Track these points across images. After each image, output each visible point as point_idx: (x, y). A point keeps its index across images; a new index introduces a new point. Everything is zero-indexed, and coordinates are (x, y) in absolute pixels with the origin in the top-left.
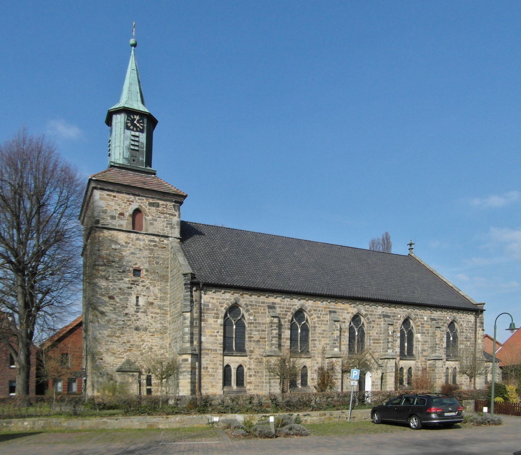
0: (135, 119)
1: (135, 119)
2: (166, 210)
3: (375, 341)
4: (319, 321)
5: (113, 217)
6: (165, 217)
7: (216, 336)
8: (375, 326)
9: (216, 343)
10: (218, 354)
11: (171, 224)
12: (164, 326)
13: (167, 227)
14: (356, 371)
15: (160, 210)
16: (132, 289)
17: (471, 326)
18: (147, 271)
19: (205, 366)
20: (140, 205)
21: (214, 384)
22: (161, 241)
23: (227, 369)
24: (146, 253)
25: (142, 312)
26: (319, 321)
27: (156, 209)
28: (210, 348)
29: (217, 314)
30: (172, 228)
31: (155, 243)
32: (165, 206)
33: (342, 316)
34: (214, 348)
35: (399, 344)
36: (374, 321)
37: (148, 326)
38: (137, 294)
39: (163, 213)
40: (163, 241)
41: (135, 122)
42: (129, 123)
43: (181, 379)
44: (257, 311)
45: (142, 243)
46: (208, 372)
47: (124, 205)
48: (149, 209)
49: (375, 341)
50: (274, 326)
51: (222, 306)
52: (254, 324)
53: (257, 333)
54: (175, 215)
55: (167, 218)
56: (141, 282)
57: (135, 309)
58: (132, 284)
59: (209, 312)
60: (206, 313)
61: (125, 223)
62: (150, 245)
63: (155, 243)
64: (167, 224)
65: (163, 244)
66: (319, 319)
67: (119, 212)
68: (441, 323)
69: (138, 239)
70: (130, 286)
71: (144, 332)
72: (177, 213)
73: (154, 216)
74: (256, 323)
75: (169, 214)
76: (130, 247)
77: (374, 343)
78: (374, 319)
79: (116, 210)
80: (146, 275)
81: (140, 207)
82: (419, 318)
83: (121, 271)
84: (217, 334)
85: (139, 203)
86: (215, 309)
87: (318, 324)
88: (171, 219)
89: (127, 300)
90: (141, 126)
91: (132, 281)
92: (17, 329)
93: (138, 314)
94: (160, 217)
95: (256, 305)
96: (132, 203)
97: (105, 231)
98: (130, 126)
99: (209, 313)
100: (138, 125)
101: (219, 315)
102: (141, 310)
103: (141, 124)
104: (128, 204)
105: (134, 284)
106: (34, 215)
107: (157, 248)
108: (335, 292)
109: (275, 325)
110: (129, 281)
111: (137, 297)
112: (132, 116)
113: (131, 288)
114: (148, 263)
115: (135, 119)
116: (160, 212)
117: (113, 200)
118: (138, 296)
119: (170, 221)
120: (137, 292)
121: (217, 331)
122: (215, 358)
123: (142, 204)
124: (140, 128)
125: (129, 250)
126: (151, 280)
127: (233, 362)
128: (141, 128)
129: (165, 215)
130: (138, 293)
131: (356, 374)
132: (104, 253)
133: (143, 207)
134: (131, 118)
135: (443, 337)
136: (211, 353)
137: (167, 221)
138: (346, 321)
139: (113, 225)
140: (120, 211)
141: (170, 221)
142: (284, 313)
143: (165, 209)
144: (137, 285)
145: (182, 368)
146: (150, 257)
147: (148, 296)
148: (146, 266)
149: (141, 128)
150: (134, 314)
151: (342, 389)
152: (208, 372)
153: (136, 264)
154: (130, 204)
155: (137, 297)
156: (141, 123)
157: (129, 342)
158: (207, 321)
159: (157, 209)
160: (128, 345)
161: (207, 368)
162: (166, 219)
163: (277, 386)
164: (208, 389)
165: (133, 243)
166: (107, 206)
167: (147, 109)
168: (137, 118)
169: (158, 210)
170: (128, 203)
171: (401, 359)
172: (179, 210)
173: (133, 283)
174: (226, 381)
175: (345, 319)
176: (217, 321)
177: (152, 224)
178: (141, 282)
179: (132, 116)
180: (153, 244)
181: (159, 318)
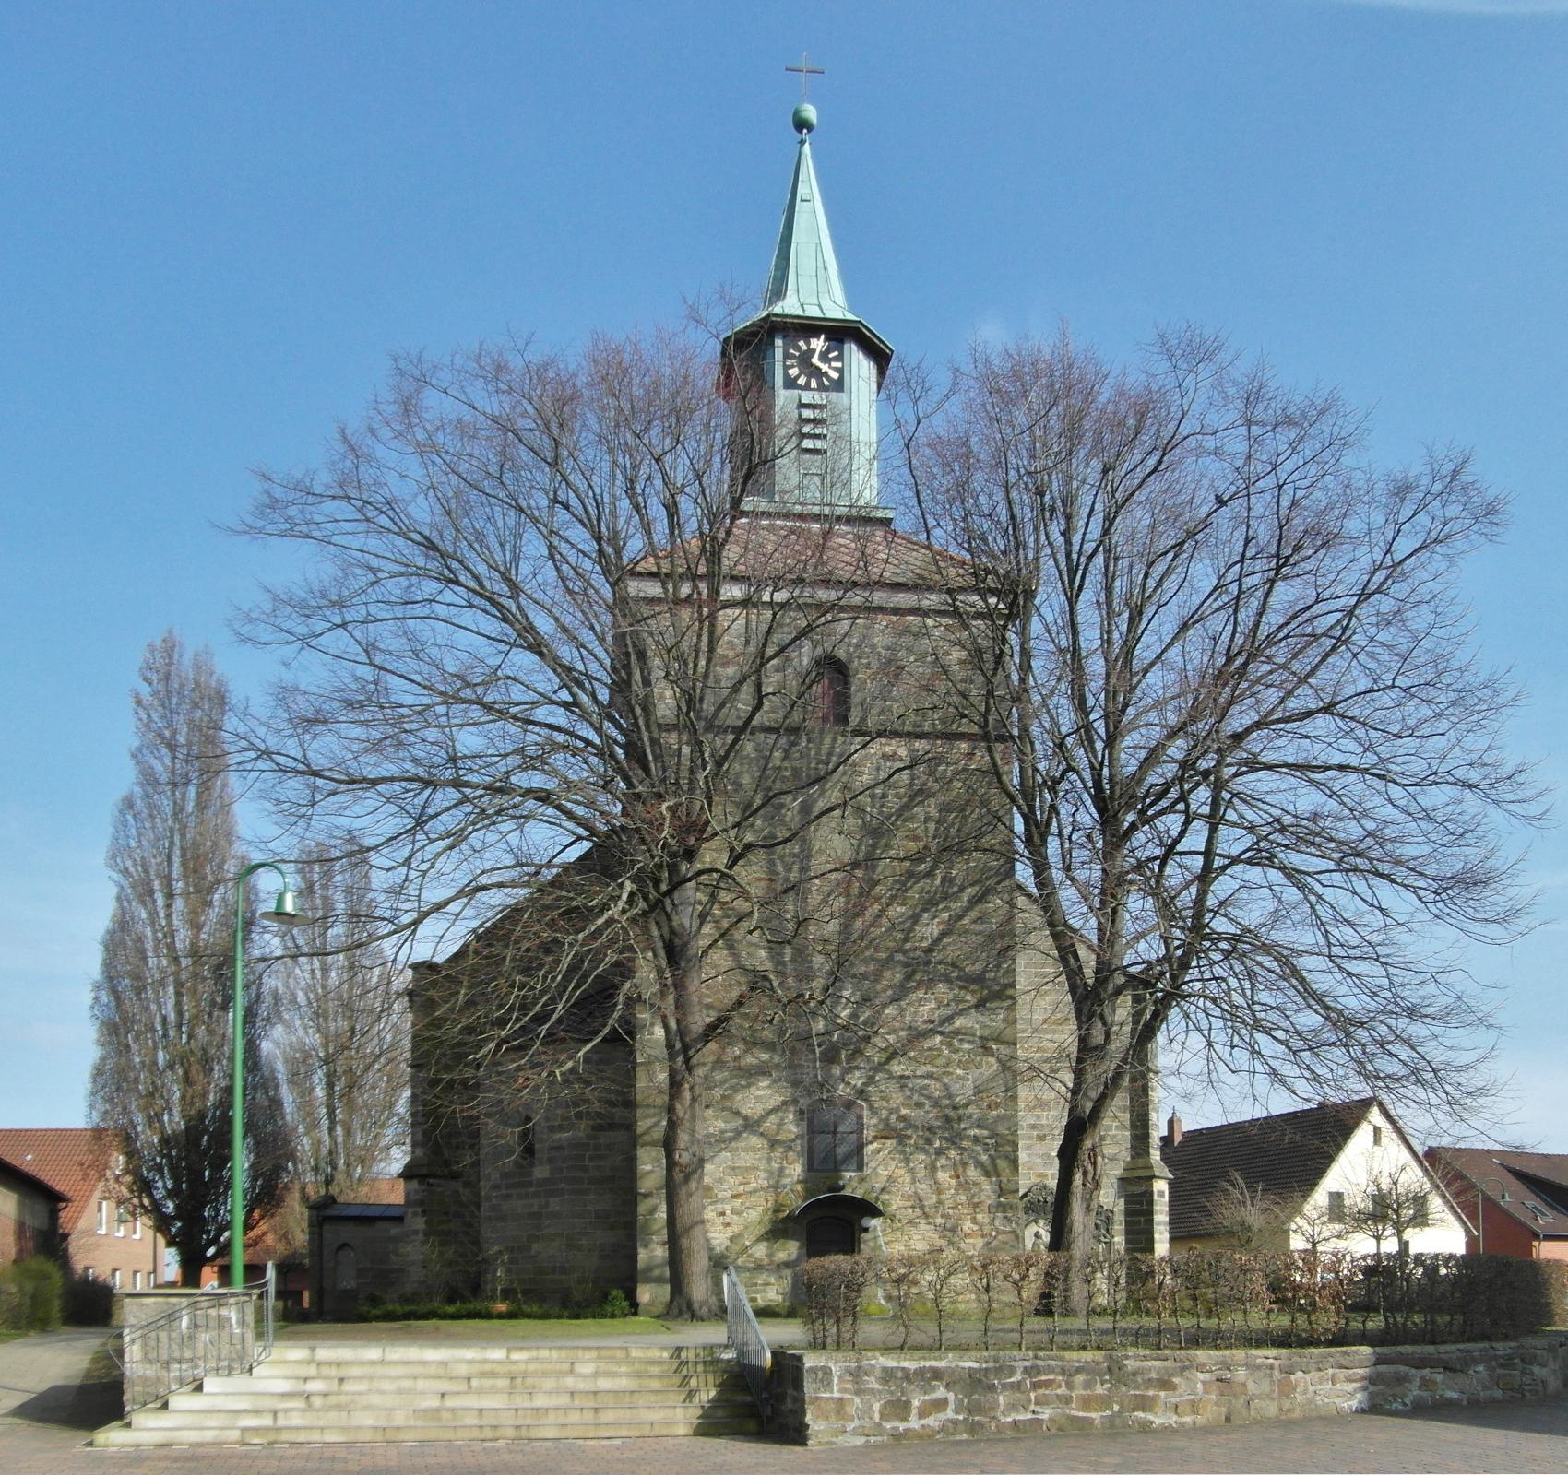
0: (812, 352)
1: (814, 351)
41: (815, 360)
42: (792, 366)
90: (836, 369)
92: (885, 1006)
98: (798, 377)
100: (824, 367)
103: (834, 364)
106: (519, 607)
108: (655, 1370)
112: (801, 343)
115: (812, 352)
124: (829, 378)
128: (835, 375)
132: (450, 1253)
134: (799, 349)
149: (835, 375)
151: (1012, 1331)
156: (836, 359)
167: (136, 1457)
168: (818, 344)
179: (801, 343)
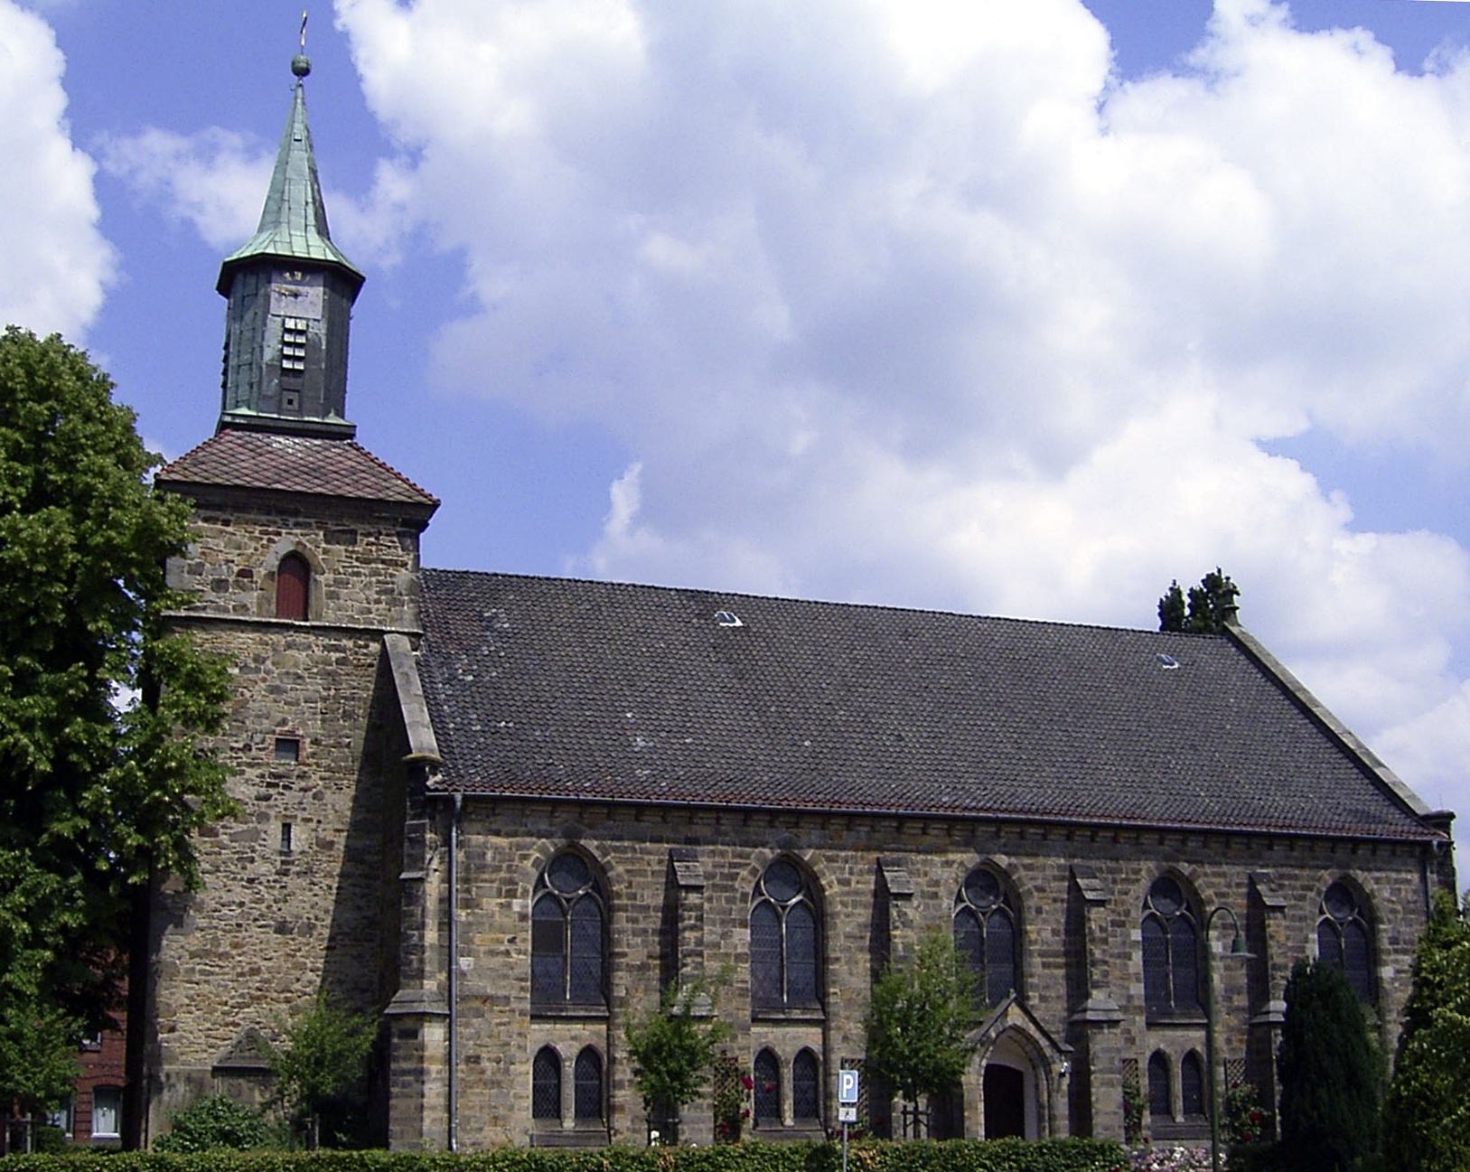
2: (377, 550)
3: (1051, 960)
4: (848, 894)
5: (220, 585)
6: (375, 573)
7: (507, 953)
8: (1046, 908)
9: (505, 977)
10: (513, 1011)
11: (392, 591)
12: (364, 918)
13: (378, 602)
14: (850, 1077)
15: (358, 552)
16: (272, 802)
17: (1410, 897)
18: (316, 742)
19: (471, 1052)
20: (299, 543)
21: (502, 1111)
22: (360, 647)
23: (548, 1059)
24: (316, 686)
25: (298, 874)
26: (848, 894)
27: (346, 551)
28: (489, 991)
29: (512, 882)
30: (395, 602)
31: (343, 655)
32: (372, 539)
33: (926, 874)
34: (501, 993)
35: (1140, 969)
36: (1041, 889)
37: (317, 918)
38: (286, 816)
39: (368, 562)
40: (366, 646)
43: (397, 1096)
44: (636, 867)
45: (302, 656)
46: (483, 1072)
47: (253, 544)
48: (325, 552)
49: (1051, 960)
50: (690, 918)
51: (525, 857)
52: (626, 911)
53: (639, 940)
54: (404, 565)
55: (380, 575)
56: (298, 777)
57: (278, 864)
58: (269, 785)
59: (486, 876)
60: (476, 880)
61: (253, 602)
62: (327, 662)
63: (343, 655)
64: (377, 593)
65: (365, 654)
66: (847, 889)
67: (236, 569)
68: (1294, 888)
69: (289, 646)
70: (263, 790)
71: (304, 940)
72: (409, 559)
73: (341, 570)
74: (632, 906)
75: (383, 562)
76: (268, 672)
77: (1045, 965)
78: (1039, 882)
79: (228, 561)
80: (313, 755)
81: (300, 549)
82: (1206, 875)
83: (240, 745)
84: (511, 947)
85: (296, 535)
86: (504, 865)
87: (844, 904)
88: (392, 575)
89: (255, 835)
91: (272, 775)
93: (285, 879)
94: (358, 574)
95: (634, 850)
96: (276, 538)
97: (199, 636)
99: (486, 881)
101: (517, 884)
102: (294, 869)
104: (265, 542)
105: (276, 785)
107: (349, 669)
109: (693, 914)
110: (263, 776)
111: (287, 828)
113: (267, 798)
114: (319, 717)
116: (357, 559)
117: (222, 532)
118: (288, 821)
119: (387, 583)
120: (286, 809)
121: (511, 936)
122: (504, 1024)
123: (304, 540)
125: (264, 680)
126: (328, 769)
127: (562, 1039)
129: (373, 565)
130: (288, 813)
131: (850, 1086)
133: (309, 545)
135: (1306, 940)
136: (492, 1011)
137: (379, 582)
138: (942, 891)
139: (218, 609)
140: (239, 564)
141: (387, 583)
142: (726, 871)
143: (374, 548)
144: (285, 787)
145: (396, 1059)
146: (324, 699)
147: (319, 822)
148: (315, 727)
150: (275, 881)
152: (483, 1072)
153: (284, 722)
154: (270, 540)
155: (287, 828)
157: (255, 971)
158: (478, 906)
159: (350, 549)
160: (255, 981)
161: (477, 1059)
162: (374, 579)
163: (700, 1120)
164: (481, 1129)
165: (276, 659)
166: (203, 553)
169: (353, 552)
170: (266, 537)
171: (1150, 1025)
172: (417, 549)
173: (276, 780)
174: (547, 1104)
175: (937, 883)
176: (509, 906)
177: (333, 596)
178: (298, 777)
180: (334, 656)
181: (351, 889)
